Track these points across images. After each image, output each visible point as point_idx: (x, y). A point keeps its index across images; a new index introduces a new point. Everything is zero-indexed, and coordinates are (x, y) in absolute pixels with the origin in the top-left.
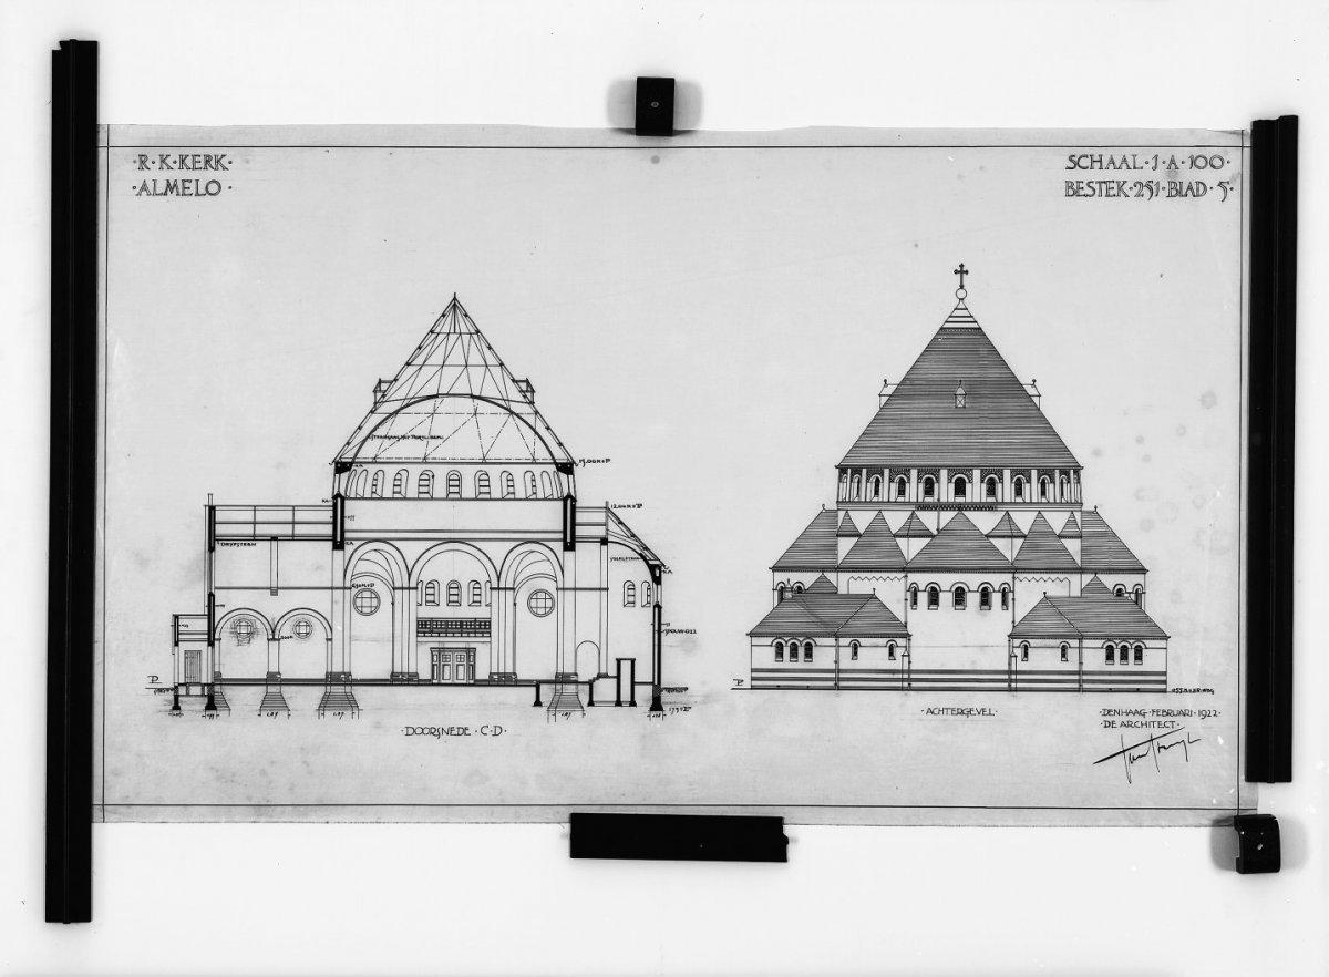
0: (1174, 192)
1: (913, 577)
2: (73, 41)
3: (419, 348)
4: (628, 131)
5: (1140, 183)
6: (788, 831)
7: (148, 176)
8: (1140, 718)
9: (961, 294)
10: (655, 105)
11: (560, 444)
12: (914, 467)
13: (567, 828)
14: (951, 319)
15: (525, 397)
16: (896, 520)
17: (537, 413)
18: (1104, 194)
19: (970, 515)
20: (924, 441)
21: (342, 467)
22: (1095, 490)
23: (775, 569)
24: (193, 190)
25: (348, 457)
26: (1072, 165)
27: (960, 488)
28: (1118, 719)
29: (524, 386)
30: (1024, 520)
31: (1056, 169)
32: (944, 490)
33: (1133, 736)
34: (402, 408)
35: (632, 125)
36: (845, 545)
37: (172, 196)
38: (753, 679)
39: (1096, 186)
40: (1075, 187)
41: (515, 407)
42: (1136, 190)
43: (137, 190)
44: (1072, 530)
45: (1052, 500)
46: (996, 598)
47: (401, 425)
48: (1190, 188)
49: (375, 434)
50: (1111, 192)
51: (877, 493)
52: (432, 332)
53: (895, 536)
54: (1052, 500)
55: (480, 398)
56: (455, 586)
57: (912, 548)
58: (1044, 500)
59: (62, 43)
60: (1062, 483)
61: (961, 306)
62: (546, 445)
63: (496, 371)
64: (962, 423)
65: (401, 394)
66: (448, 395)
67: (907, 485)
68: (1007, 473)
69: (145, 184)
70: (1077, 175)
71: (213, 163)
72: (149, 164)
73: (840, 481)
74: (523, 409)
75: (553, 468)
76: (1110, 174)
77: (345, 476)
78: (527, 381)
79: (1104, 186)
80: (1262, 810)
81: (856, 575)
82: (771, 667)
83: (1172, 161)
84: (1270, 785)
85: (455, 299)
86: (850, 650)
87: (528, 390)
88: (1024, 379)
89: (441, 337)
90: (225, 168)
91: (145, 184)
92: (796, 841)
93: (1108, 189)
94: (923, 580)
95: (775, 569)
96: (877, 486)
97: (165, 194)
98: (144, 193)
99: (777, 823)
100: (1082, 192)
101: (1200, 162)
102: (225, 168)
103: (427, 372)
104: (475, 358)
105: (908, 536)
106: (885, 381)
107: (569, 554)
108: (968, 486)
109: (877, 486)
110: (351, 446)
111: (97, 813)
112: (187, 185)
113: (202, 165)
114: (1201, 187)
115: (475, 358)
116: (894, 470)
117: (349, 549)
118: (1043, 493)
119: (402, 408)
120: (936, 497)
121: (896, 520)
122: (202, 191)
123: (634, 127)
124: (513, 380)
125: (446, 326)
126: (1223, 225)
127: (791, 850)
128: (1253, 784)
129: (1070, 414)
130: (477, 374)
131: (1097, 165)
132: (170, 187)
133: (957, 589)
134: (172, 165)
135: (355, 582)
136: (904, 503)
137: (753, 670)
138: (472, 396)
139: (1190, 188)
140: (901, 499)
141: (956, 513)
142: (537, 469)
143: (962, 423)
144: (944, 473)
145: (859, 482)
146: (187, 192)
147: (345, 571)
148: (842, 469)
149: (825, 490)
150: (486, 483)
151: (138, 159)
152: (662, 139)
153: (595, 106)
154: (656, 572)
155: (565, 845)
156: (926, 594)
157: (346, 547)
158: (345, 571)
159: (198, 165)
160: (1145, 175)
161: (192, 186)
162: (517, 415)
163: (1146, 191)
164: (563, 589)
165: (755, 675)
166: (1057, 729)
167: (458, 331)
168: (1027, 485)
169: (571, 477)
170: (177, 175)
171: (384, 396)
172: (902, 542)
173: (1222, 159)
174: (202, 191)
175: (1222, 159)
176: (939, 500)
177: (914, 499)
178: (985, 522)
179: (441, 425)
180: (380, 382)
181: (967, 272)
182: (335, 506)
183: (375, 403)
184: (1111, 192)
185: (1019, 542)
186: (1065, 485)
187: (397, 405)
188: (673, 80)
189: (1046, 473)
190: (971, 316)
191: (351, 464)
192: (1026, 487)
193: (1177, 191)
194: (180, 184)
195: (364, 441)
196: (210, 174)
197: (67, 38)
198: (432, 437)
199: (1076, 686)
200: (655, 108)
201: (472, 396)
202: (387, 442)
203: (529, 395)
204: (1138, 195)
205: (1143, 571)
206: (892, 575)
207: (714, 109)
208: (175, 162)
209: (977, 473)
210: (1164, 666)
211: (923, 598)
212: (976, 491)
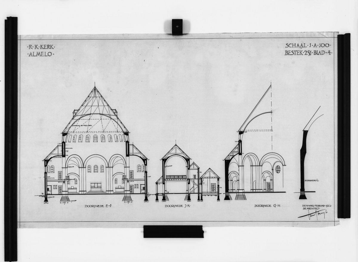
2: (11, 17)
3: (85, 101)
4: (170, 34)
5: (306, 51)
6: (204, 229)
11: (125, 127)
13: (142, 229)
15: (115, 114)
17: (118, 118)
18: (296, 54)
21: (64, 134)
24: (44, 55)
25: (242, 130)
26: (287, 46)
29: (114, 111)
31: (281, 46)
34: (81, 118)
35: (171, 32)
37: (38, 57)
39: (294, 52)
40: (288, 52)
41: (112, 117)
47: (80, 122)
48: (320, 52)
49: (74, 125)
50: (299, 54)
52: (89, 96)
55: (102, 114)
56: (96, 166)
59: (7, 18)
62: (121, 128)
63: (107, 107)
65: (81, 114)
66: (93, 114)
70: (288, 49)
71: (50, 47)
74: (115, 117)
75: (123, 133)
77: (65, 137)
78: (115, 110)
79: (296, 52)
83: (315, 45)
85: (95, 87)
87: (115, 112)
89: (91, 98)
90: (53, 49)
92: (206, 232)
99: (200, 227)
100: (290, 54)
102: (53, 49)
103: (87, 108)
104: (101, 104)
107: (128, 157)
110: (67, 129)
112: (43, 53)
113: (47, 48)
115: (101, 104)
117: (67, 157)
119: (81, 118)
124: (111, 109)
125: (93, 95)
127: (205, 234)
130: (101, 108)
131: (294, 46)
132: (38, 54)
134: (38, 48)
135: (69, 166)
138: (100, 114)
139: (320, 52)
142: (118, 134)
147: (242, 163)
150: (104, 138)
153: (160, 27)
154: (145, 160)
155: (142, 234)
157: (66, 156)
158: (242, 163)
162: (113, 119)
164: (126, 167)
167: (96, 96)
169: (128, 136)
170: (40, 51)
171: (76, 114)
173: (329, 45)
174: (47, 55)
175: (329, 45)
179: (92, 122)
180: (75, 110)
182: (63, 145)
183: (74, 116)
187: (79, 117)
188: (182, 20)
191: (243, 132)
193: (316, 53)
194: (41, 53)
195: (70, 127)
198: (89, 126)
200: (177, 27)
201: (100, 114)
202: (77, 127)
203: (116, 113)
204: (305, 54)
207: (193, 28)
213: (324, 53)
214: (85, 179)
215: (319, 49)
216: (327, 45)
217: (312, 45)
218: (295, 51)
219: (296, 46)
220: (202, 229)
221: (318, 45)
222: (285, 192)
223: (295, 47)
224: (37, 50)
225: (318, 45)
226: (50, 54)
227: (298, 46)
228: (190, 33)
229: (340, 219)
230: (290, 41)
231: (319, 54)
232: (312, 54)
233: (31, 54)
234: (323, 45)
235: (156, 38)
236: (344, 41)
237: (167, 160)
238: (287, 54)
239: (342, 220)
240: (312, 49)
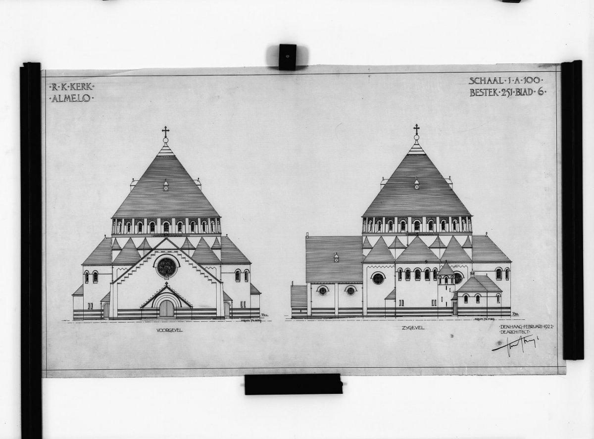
1: (398, 266)
5: (504, 90)
6: (343, 379)
7: (57, 93)
8: (518, 329)
9: (417, 137)
10: (288, 56)
12: (438, 216)
14: (412, 150)
16: (389, 240)
19: (421, 237)
20: (147, 207)
22: (226, 227)
23: (84, 265)
24: (77, 99)
26: (472, 82)
27: (166, 228)
28: (506, 330)
30: (446, 240)
32: (159, 228)
33: (512, 338)
35: (276, 64)
36: (115, 254)
38: (293, 313)
39: (484, 91)
42: (502, 93)
43: (52, 100)
44: (217, 246)
45: (448, 231)
46: (242, 276)
48: (525, 91)
51: (379, 229)
53: (138, 249)
54: (458, 231)
57: (397, 253)
58: (193, 232)
60: (463, 223)
61: (417, 143)
64: (418, 194)
67: (143, 226)
68: (174, 220)
70: (475, 87)
71: (86, 87)
72: (57, 87)
73: (363, 224)
81: (370, 265)
82: (474, 306)
83: (517, 80)
86: (463, 299)
88: (445, 176)
92: (346, 384)
93: (490, 92)
94: (404, 267)
95: (84, 265)
96: (129, 227)
97: (65, 101)
99: (337, 377)
101: (530, 80)
105: (395, 248)
106: (133, 179)
108: (170, 227)
109: (129, 227)
111: (44, 372)
112: (74, 97)
114: (530, 91)
116: (137, 220)
118: (455, 228)
120: (406, 231)
121: (389, 240)
123: (278, 66)
126: (547, 108)
127: (344, 388)
129: (216, 194)
131: (483, 82)
133: (416, 271)
136: (142, 234)
137: (75, 311)
139: (525, 91)
140: (140, 233)
141: (415, 237)
143: (418, 194)
144: (410, 219)
145: (121, 225)
146: (74, 100)
148: (114, 219)
149: (107, 229)
151: (52, 86)
152: (293, 72)
153: (259, 56)
156: (433, 273)
160: (506, 86)
161: (76, 97)
163: (507, 93)
165: (75, 313)
166: (473, 335)
168: (184, 226)
170: (69, 92)
172: (392, 251)
174: (81, 100)
176: (407, 232)
177: (396, 231)
178: (429, 241)
181: (419, 128)
185: (443, 250)
186: (464, 224)
188: (295, 46)
189: (204, 220)
190: (421, 148)
192: (446, 225)
193: (519, 92)
196: (85, 92)
199: (394, 314)
200: (288, 58)
205: (510, 262)
206: (388, 265)
207: (316, 55)
208: (68, 87)
209: (174, 220)
210: (362, 305)
211: (91, 277)
212: (424, 227)
213: (532, 93)
215: (522, 86)
217: (50, 98)
219: (486, 82)
220: (339, 379)
221: (522, 80)
223: (485, 83)
226: (86, 98)
227: (495, 82)
228: (309, 65)
229: (567, 361)
231: (525, 93)
232: (514, 94)
233: (55, 98)
235: (255, 73)
236: (571, 75)
238: (473, 94)
239: (570, 364)
240: (514, 86)
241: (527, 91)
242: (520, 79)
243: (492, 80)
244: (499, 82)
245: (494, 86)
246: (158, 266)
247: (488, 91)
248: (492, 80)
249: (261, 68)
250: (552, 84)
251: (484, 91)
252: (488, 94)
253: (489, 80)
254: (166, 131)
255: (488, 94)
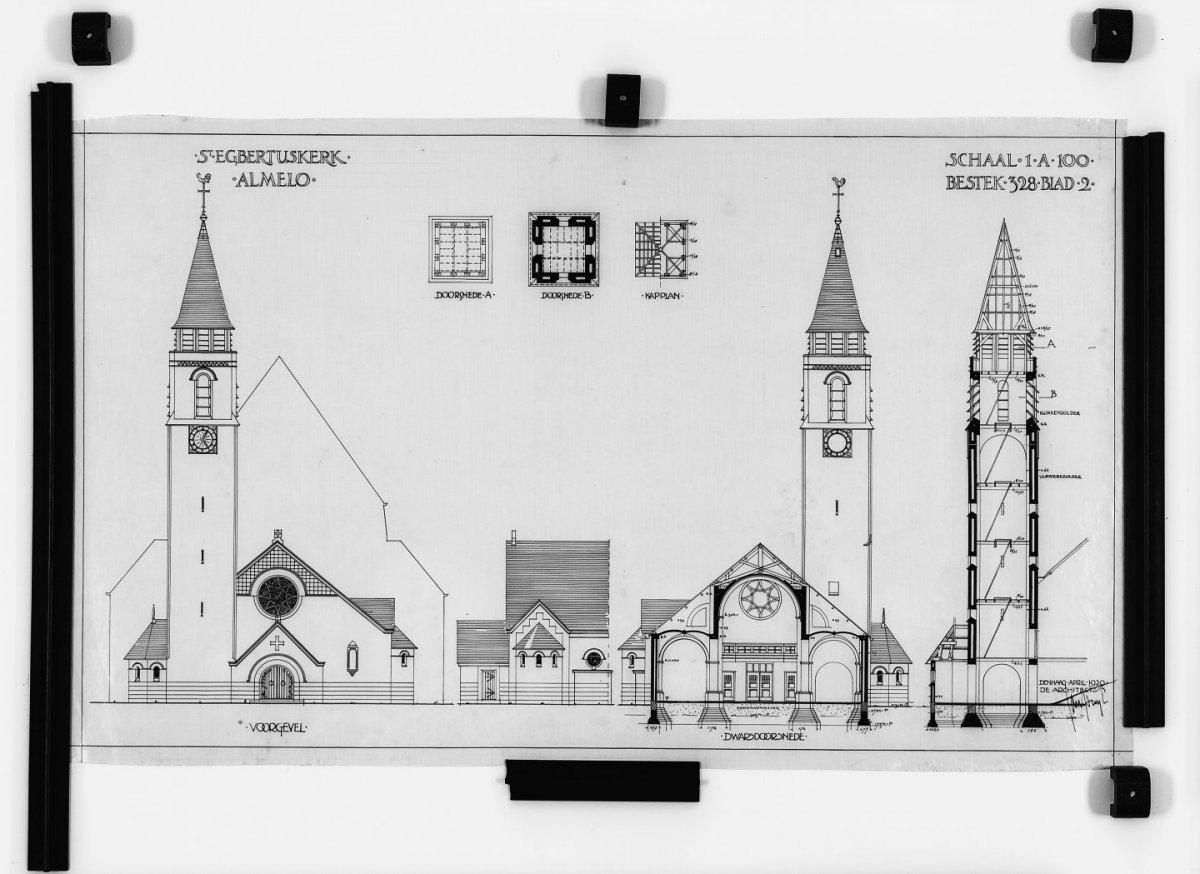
0: (1046, 186)
2: (49, 83)
4: (600, 122)
39: (975, 181)
43: (236, 182)
48: (1059, 182)
50: (989, 186)
59: (40, 85)
69: (243, 176)
70: (956, 171)
76: (988, 170)
79: (982, 181)
80: (1137, 760)
83: (1044, 158)
84: (1145, 730)
91: (243, 176)
98: (243, 184)
99: (517, 794)
101: (1069, 160)
122: (293, 182)
127: (704, 790)
128: (1129, 729)
131: (975, 163)
132: (267, 180)
153: (571, 99)
159: (315, 160)
160: (1021, 171)
174: (293, 182)
184: (989, 186)
188: (1093, 60)
193: (1050, 185)
197: (44, 81)
207: (674, 101)
214: (536, 685)
215: (1055, 172)
216: (1083, 161)
218: (978, 178)
222: (203, 499)
224: (1044, 171)
225: (1035, 160)
230: (958, 147)
234: (1069, 160)
237: (729, 593)
240: (1038, 173)
241: (1063, 181)
242: (1049, 159)
243: (995, 159)
244: (1007, 164)
245: (999, 171)
246: (261, 593)
247: (982, 181)
248: (995, 159)
249: (568, 121)
250: (1107, 174)
251: (290, 158)
252: (982, 185)
253: (988, 159)
254: (839, 194)
255: (982, 185)
